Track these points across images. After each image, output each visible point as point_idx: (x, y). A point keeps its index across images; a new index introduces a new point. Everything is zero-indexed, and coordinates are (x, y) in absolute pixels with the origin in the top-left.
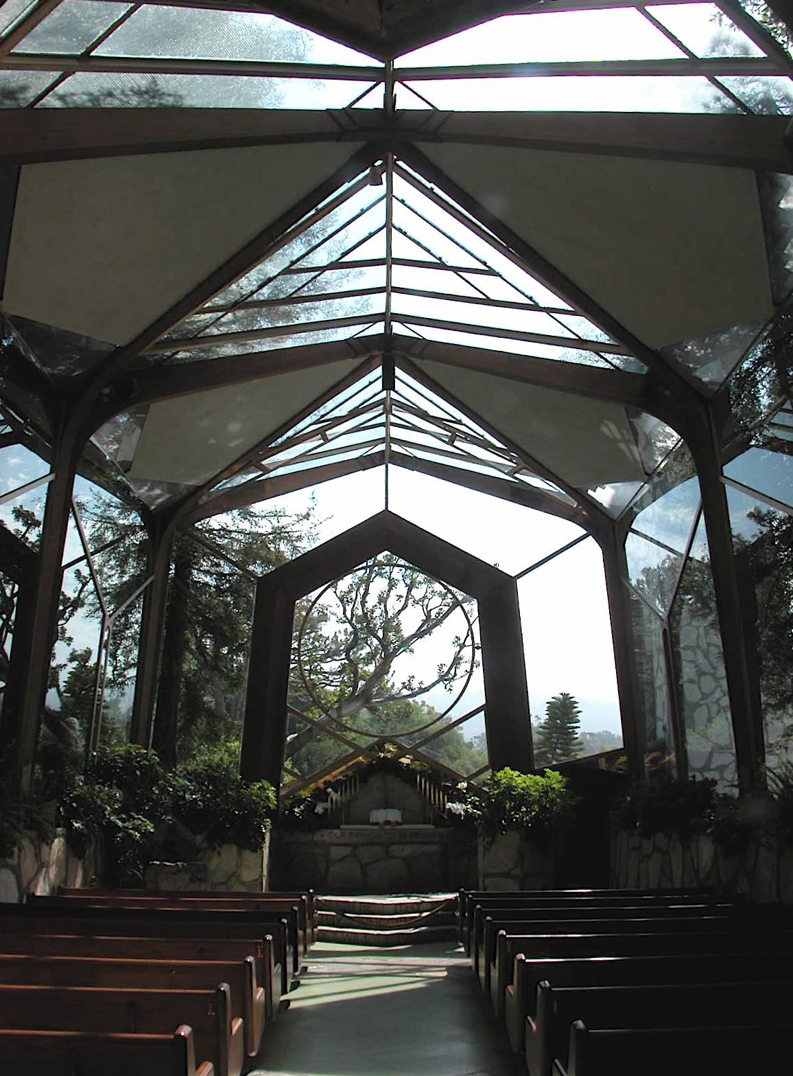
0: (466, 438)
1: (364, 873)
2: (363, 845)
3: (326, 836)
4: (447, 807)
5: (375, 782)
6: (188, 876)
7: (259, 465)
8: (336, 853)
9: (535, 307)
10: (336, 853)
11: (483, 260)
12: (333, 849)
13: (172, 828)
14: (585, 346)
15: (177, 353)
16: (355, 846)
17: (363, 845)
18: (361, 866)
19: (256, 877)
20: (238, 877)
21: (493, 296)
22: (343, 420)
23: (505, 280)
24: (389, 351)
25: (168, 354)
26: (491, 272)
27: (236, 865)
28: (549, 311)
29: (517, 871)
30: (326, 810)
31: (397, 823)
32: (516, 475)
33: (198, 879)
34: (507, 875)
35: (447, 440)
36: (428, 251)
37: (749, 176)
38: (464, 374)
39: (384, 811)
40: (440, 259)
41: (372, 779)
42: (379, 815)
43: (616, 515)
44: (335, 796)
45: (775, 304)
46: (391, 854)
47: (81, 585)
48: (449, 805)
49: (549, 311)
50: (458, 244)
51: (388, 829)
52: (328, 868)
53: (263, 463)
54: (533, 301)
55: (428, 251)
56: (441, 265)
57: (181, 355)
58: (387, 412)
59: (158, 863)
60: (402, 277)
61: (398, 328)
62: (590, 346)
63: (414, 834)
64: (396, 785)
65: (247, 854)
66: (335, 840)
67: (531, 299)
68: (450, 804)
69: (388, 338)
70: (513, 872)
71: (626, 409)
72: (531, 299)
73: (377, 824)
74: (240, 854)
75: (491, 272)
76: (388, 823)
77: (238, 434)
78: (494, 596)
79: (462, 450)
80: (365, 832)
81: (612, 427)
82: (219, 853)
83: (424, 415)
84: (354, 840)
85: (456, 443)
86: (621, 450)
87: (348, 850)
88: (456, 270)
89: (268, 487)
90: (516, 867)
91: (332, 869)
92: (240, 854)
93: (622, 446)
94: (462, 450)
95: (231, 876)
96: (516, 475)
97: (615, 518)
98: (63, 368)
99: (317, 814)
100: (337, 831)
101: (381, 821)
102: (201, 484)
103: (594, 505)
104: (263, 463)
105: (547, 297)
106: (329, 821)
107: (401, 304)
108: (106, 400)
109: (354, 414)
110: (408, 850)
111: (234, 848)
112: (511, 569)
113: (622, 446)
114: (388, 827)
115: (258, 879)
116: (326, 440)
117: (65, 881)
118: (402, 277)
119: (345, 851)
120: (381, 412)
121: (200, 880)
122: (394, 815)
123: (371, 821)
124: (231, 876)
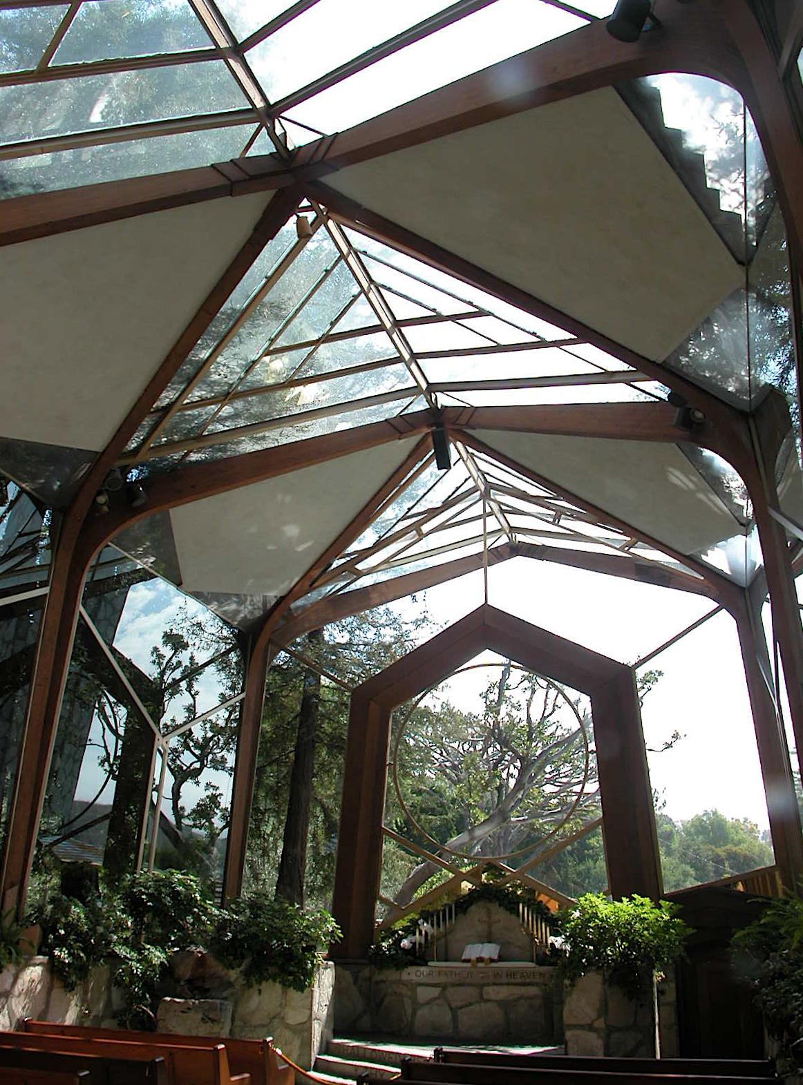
0: (571, 516)
1: (455, 1019)
2: (453, 985)
3: (413, 974)
4: (549, 942)
5: (477, 912)
6: (200, 1016)
7: (353, 570)
8: (424, 994)
9: (542, 344)
10: (424, 994)
11: (468, 300)
12: (419, 989)
13: (201, 961)
14: (613, 379)
15: (187, 454)
16: (444, 987)
17: (453, 985)
18: (451, 1009)
19: (305, 1020)
20: (283, 1018)
21: (504, 341)
22: (440, 511)
23: (497, 317)
24: (439, 429)
25: (177, 456)
26: (481, 313)
27: (281, 1005)
28: (557, 344)
29: (600, 1024)
30: (414, 944)
31: (492, 960)
32: (632, 550)
33: (210, 1019)
34: (590, 1027)
35: (551, 520)
36: (420, 304)
37: (607, 97)
38: (529, 439)
39: (481, 945)
40: (434, 310)
41: (473, 908)
42: (474, 951)
43: (743, 581)
44: (425, 927)
45: (740, 262)
46: (485, 997)
47: (228, 713)
48: (551, 939)
49: (557, 344)
50: (436, 288)
51: (480, 968)
52: (414, 1013)
53: (357, 567)
54: (538, 337)
55: (420, 304)
56: (437, 318)
57: (194, 457)
58: (485, 496)
59: (182, 1000)
60: (420, 338)
61: (444, 400)
62: (617, 378)
63: (511, 973)
64: (500, 914)
65: (292, 993)
66: (422, 980)
67: (534, 334)
68: (552, 938)
69: (435, 415)
70: (596, 1025)
71: (677, 445)
72: (534, 334)
73: (468, 961)
74: (284, 993)
75: (481, 313)
76: (480, 960)
77: (300, 537)
78: (615, 692)
79: (568, 529)
80: (454, 970)
81: (678, 473)
82: (260, 991)
83: (524, 496)
84: (443, 979)
85: (562, 522)
86: (701, 501)
87: (435, 992)
88: (454, 318)
89: (375, 597)
90: (599, 1017)
91: (419, 1013)
92: (284, 993)
93: (701, 496)
94: (568, 529)
95: (274, 1018)
96: (632, 550)
97: (744, 586)
98: (42, 481)
99: (403, 949)
100: (423, 969)
101: (473, 958)
102: (282, 594)
103: (711, 573)
104: (357, 567)
105: (552, 332)
106: (417, 957)
107: (437, 371)
108: (105, 509)
109: (447, 504)
110: (503, 993)
111: (278, 987)
112: (624, 655)
113: (701, 496)
114: (481, 965)
115: (305, 1023)
116: (421, 536)
117: (43, 1015)
118: (420, 338)
119: (435, 992)
120: (478, 498)
121: (213, 1021)
122: (489, 950)
123: (463, 958)
124: (274, 1018)
